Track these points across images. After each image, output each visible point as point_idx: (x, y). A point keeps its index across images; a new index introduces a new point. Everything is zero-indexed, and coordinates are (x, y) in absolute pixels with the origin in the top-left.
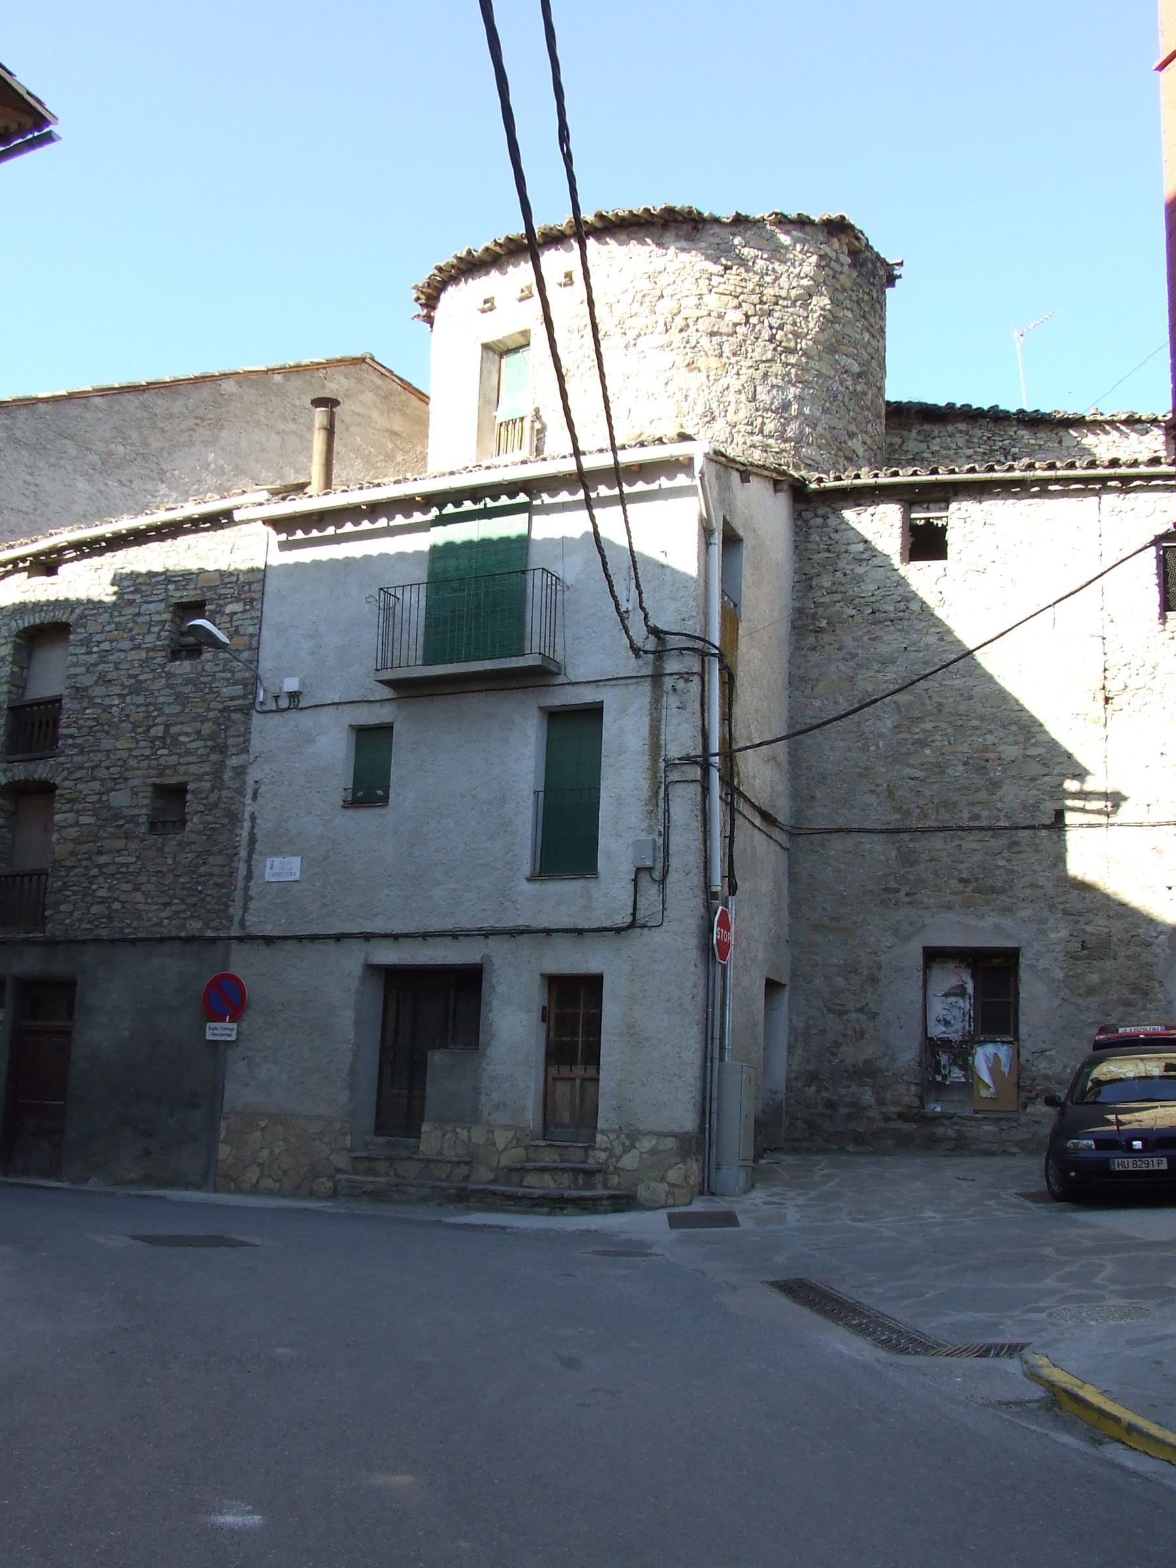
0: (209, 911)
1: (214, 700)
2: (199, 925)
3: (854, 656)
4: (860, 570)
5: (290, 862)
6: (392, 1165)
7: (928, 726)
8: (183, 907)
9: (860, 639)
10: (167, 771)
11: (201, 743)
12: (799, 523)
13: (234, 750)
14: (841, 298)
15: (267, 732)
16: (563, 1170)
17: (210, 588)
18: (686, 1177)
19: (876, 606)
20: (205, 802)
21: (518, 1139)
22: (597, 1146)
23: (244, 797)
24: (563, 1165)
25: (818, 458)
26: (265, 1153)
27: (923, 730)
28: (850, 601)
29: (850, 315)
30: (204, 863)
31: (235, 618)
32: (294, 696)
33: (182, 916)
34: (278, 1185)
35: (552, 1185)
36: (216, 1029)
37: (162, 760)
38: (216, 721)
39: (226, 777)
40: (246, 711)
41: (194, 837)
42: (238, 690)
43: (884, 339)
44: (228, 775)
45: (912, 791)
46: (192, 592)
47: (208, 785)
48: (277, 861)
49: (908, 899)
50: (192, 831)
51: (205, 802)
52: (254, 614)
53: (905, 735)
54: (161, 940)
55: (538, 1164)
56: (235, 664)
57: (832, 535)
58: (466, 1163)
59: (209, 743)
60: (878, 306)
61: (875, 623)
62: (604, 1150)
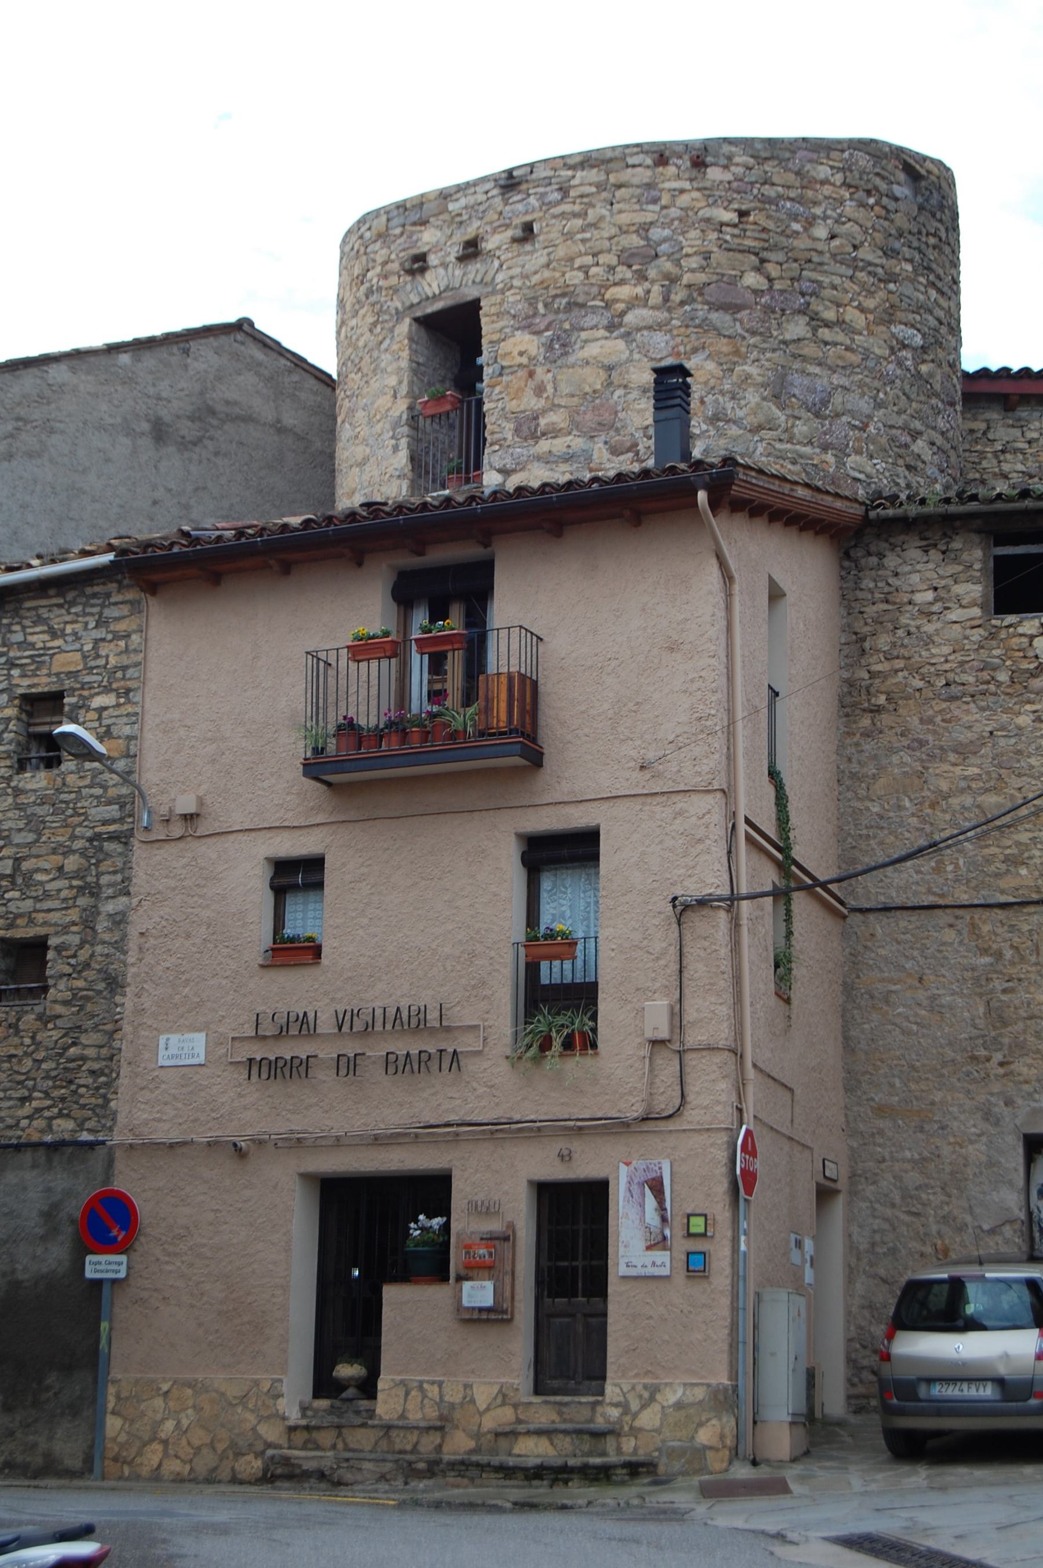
0: (83, 1107)
1: (80, 825)
2: (70, 1125)
3: (922, 743)
4: (929, 628)
5: (191, 1040)
6: (340, 1435)
7: (1024, 837)
8: (49, 1102)
9: (930, 721)
10: (19, 921)
11: (64, 883)
12: (846, 564)
13: (110, 891)
14: (897, 245)
15: (150, 866)
16: (565, 1432)
17: (69, 674)
18: (722, 1437)
19: (951, 676)
20: (73, 961)
21: (504, 1396)
22: (608, 1400)
23: (125, 953)
24: (563, 1426)
25: (869, 469)
26: (169, 1425)
27: (1018, 844)
28: (916, 670)
29: (909, 267)
30: (74, 1044)
31: (105, 714)
32: (189, 818)
33: (47, 1114)
34: (188, 1467)
35: (551, 1451)
36: (100, 1263)
37: (12, 907)
38: (83, 853)
39: (99, 928)
40: (123, 838)
41: (59, 1009)
42: (113, 811)
43: (957, 293)
44: (102, 925)
45: (1003, 924)
46: (45, 680)
47: (75, 940)
48: (174, 1038)
49: (1001, 1071)
50: (55, 1002)
51: (73, 961)
52: (130, 709)
53: (993, 850)
54: (18, 1148)
55: (532, 1427)
56: (107, 776)
57: (890, 581)
58: (436, 1429)
59: (75, 883)
60: (947, 250)
61: (952, 699)
62: (617, 1405)
